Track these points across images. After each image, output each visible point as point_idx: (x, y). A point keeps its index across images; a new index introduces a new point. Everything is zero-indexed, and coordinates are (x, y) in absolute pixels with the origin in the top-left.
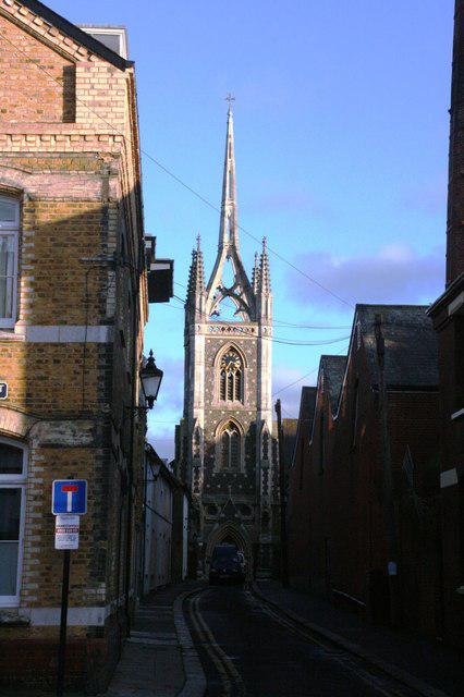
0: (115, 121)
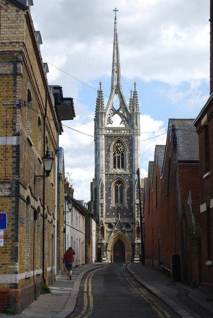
0: (20, 35)
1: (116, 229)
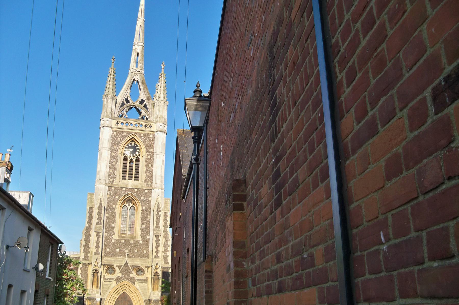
1: (120, 275)
